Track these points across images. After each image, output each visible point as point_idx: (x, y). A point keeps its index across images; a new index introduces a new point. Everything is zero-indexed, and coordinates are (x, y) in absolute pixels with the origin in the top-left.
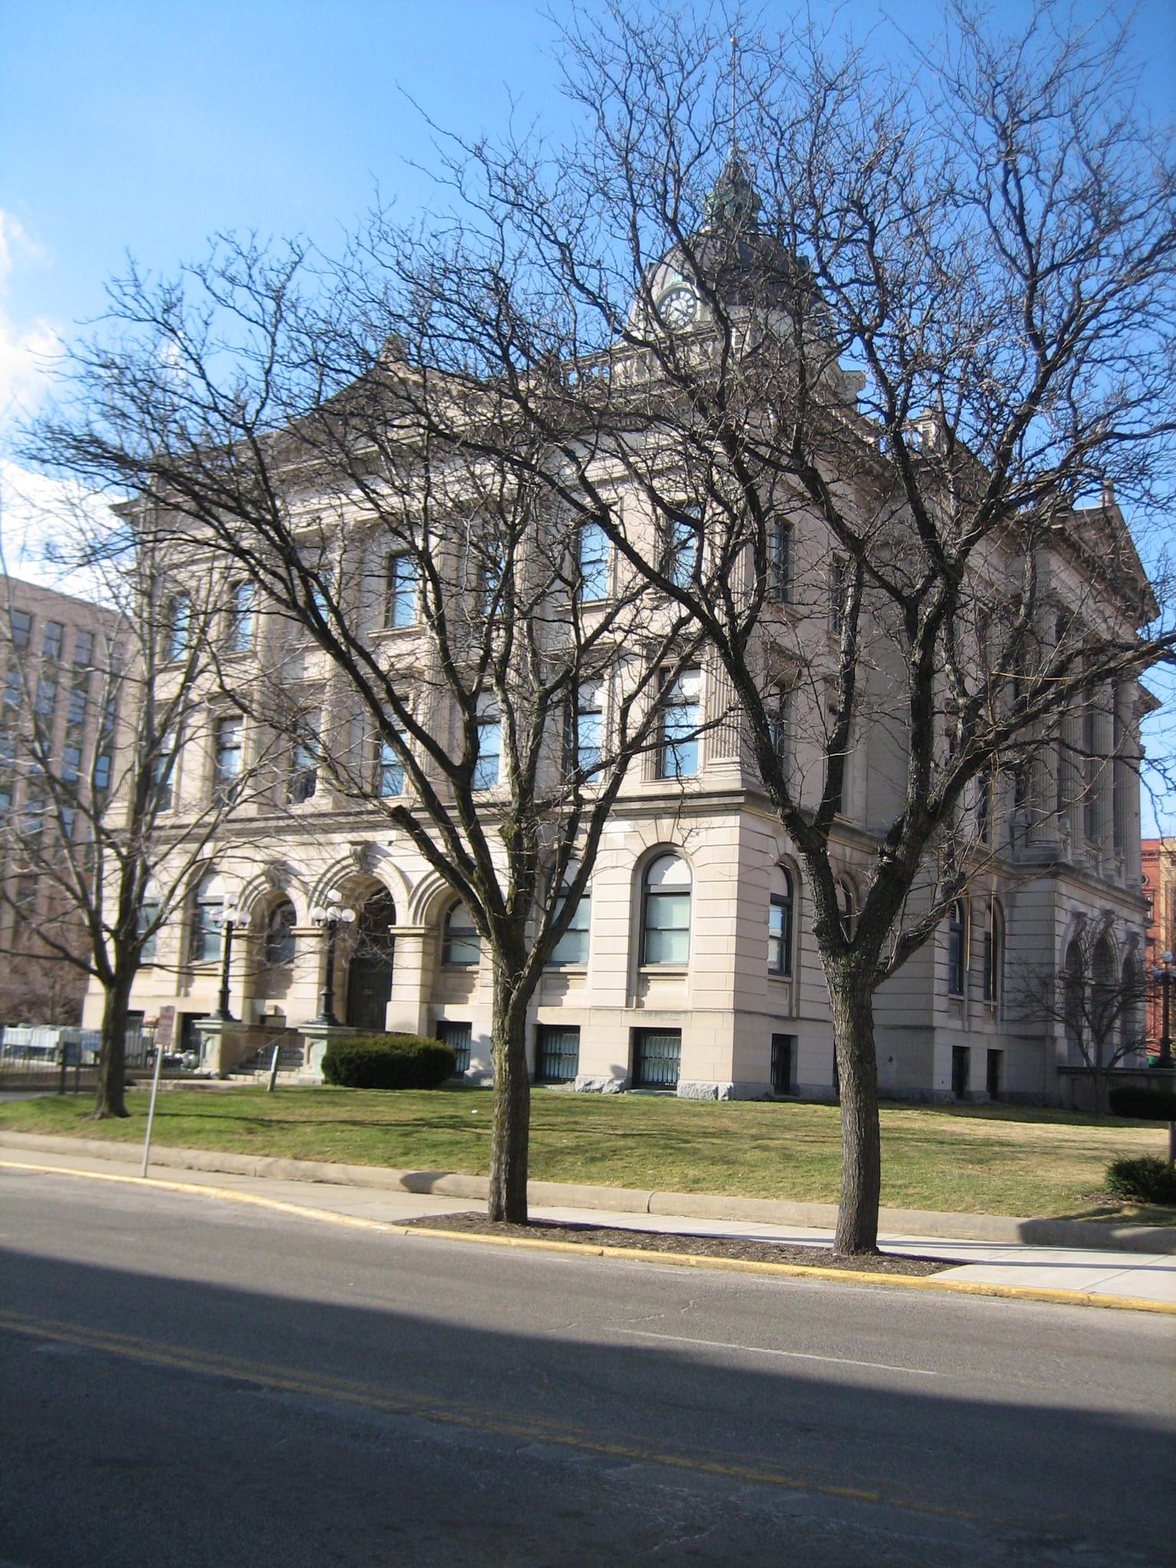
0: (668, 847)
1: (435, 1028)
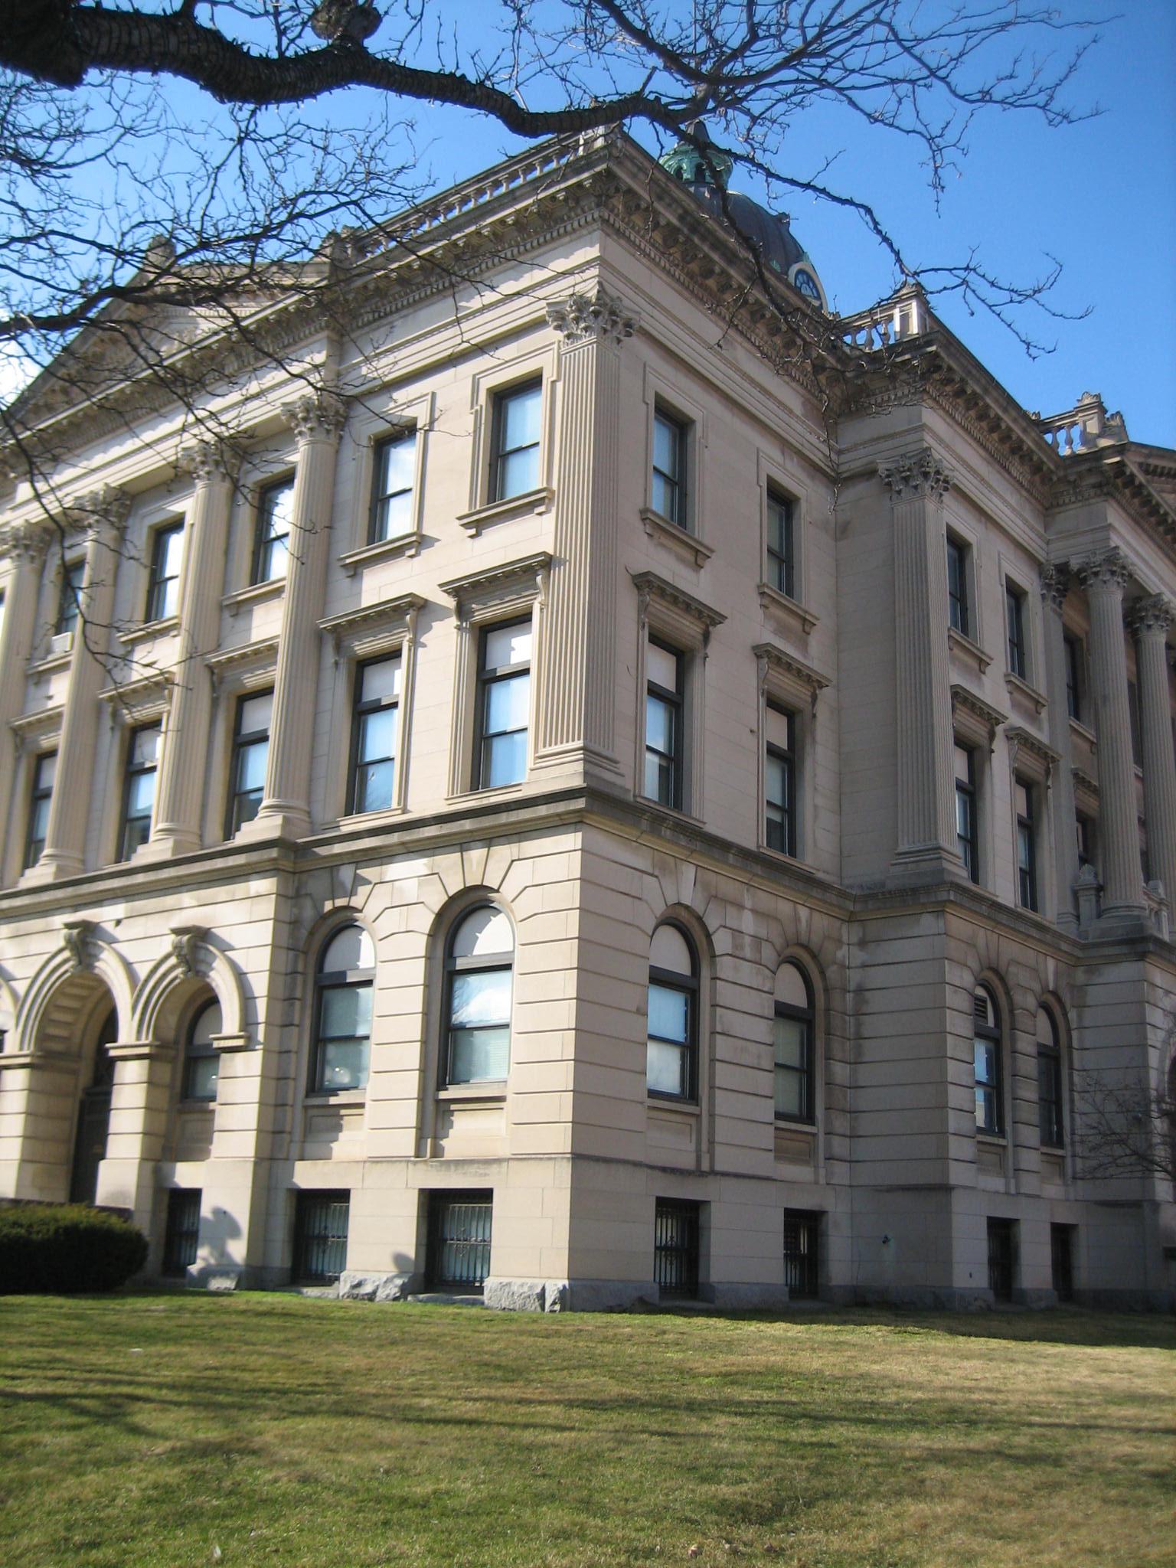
1: (166, 1199)
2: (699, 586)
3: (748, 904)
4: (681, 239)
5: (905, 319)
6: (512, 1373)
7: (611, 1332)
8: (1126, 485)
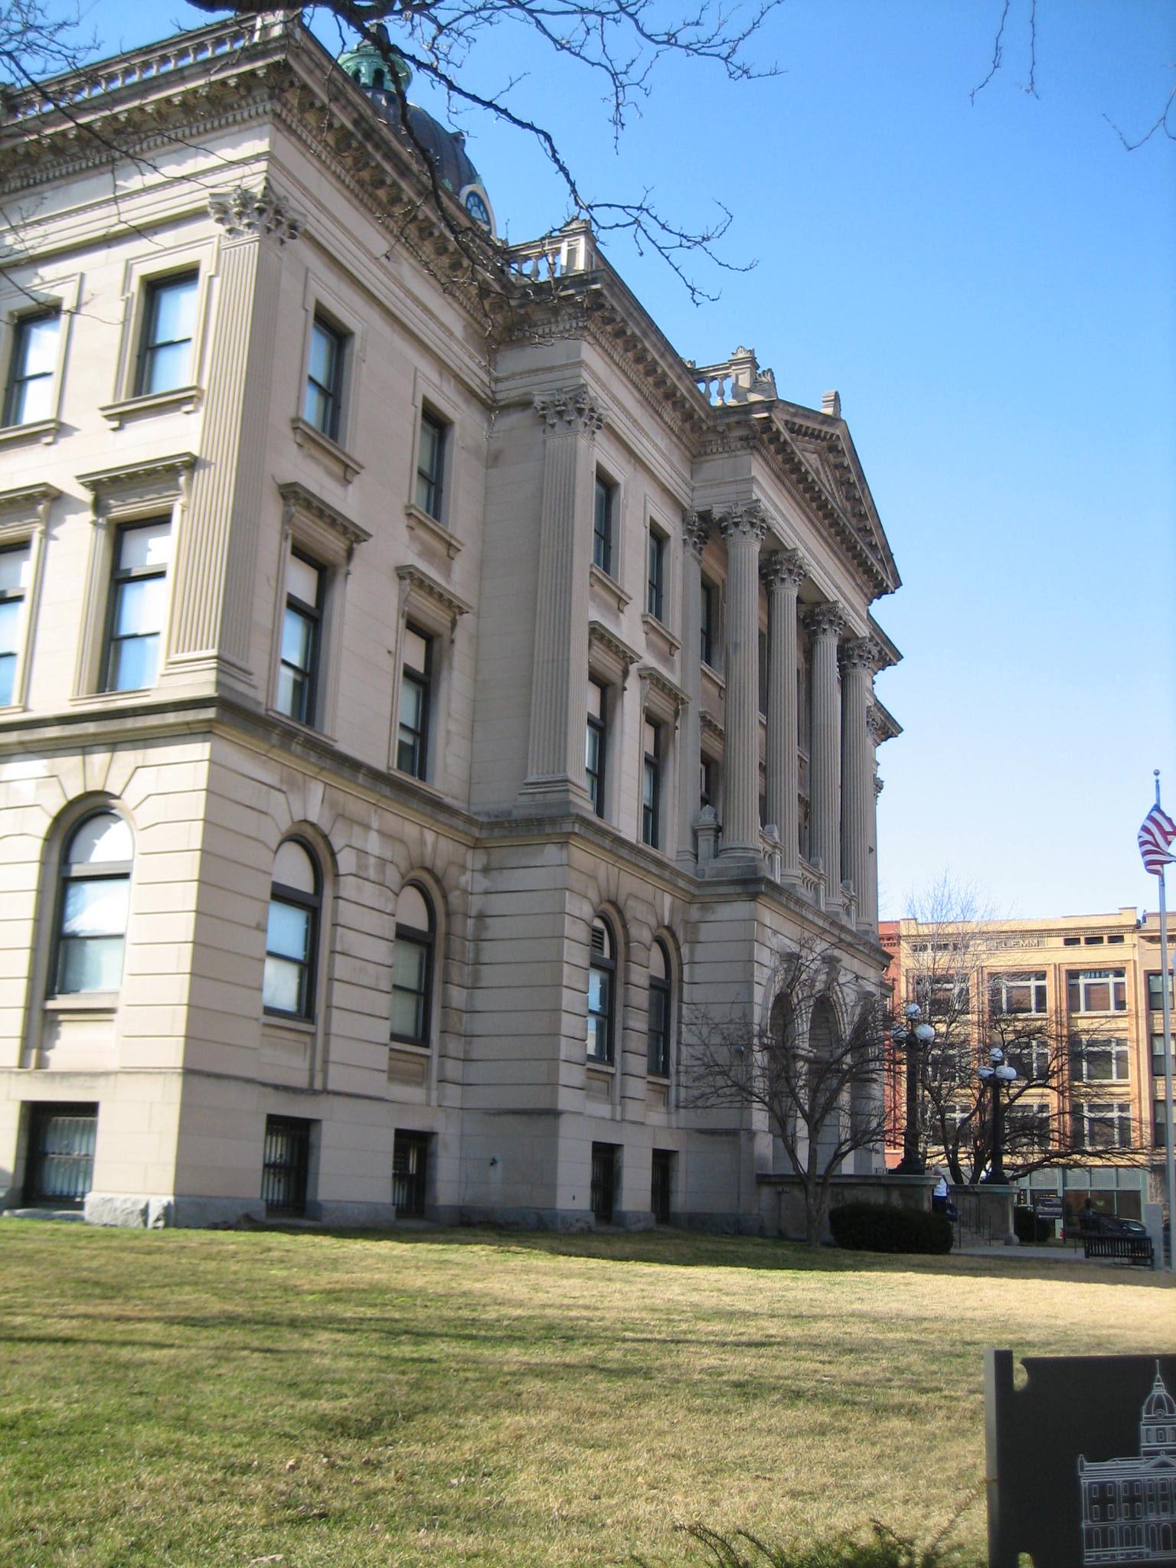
0: (100, 800)
2: (347, 501)
3: (375, 825)
4: (354, 144)
5: (572, 253)
6: (112, 1290)
7: (215, 1249)
8: (771, 441)
